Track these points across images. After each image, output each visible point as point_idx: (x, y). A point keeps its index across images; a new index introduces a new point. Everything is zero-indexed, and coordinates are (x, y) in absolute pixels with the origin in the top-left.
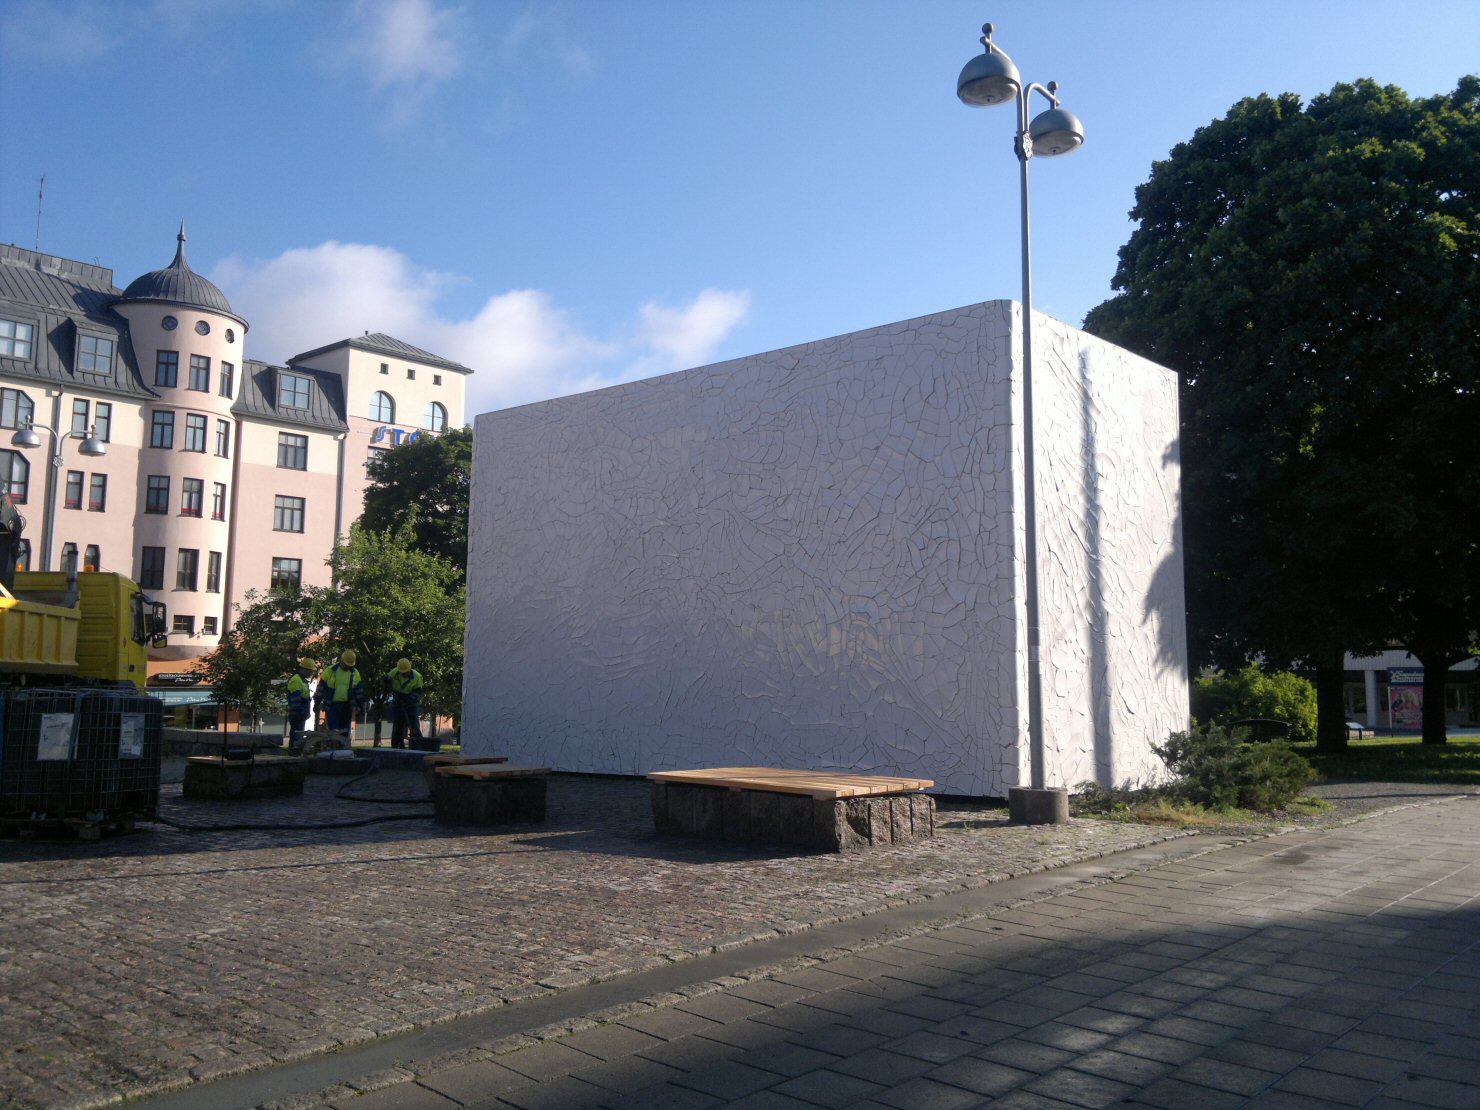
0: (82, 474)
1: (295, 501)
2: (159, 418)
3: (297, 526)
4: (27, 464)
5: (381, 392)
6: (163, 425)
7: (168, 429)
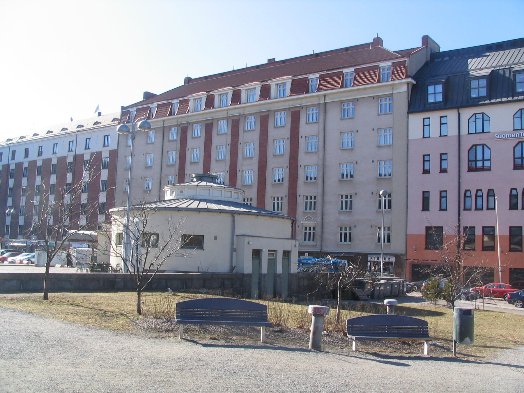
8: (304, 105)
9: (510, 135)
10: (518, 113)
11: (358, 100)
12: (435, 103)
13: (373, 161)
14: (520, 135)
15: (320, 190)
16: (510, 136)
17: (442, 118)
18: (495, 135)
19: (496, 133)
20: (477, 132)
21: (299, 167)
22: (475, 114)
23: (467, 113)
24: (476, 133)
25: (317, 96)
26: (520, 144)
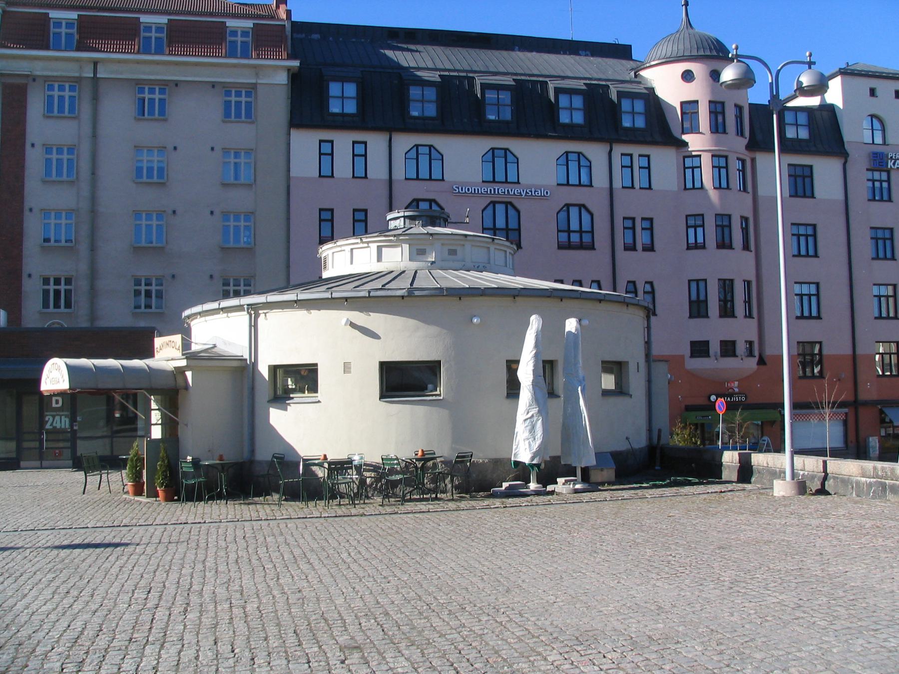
0: (633, 219)
1: (808, 227)
2: (688, 163)
3: (889, 255)
4: (518, 212)
5: (872, 116)
6: (693, 168)
7: (697, 171)
8: (38, 73)
9: (478, 189)
10: (411, 151)
11: (176, 84)
12: (343, 115)
13: (212, 213)
14: (495, 192)
15: (83, 267)
16: (478, 191)
17: (686, 159)
18: (454, 187)
19: (455, 183)
20: (696, 187)
21: (27, 213)
22: (417, 146)
23: (404, 142)
24: (430, 179)
25: (77, 60)
26: (492, 205)
